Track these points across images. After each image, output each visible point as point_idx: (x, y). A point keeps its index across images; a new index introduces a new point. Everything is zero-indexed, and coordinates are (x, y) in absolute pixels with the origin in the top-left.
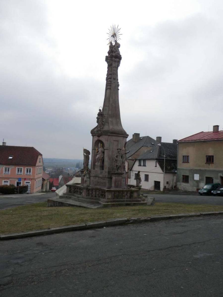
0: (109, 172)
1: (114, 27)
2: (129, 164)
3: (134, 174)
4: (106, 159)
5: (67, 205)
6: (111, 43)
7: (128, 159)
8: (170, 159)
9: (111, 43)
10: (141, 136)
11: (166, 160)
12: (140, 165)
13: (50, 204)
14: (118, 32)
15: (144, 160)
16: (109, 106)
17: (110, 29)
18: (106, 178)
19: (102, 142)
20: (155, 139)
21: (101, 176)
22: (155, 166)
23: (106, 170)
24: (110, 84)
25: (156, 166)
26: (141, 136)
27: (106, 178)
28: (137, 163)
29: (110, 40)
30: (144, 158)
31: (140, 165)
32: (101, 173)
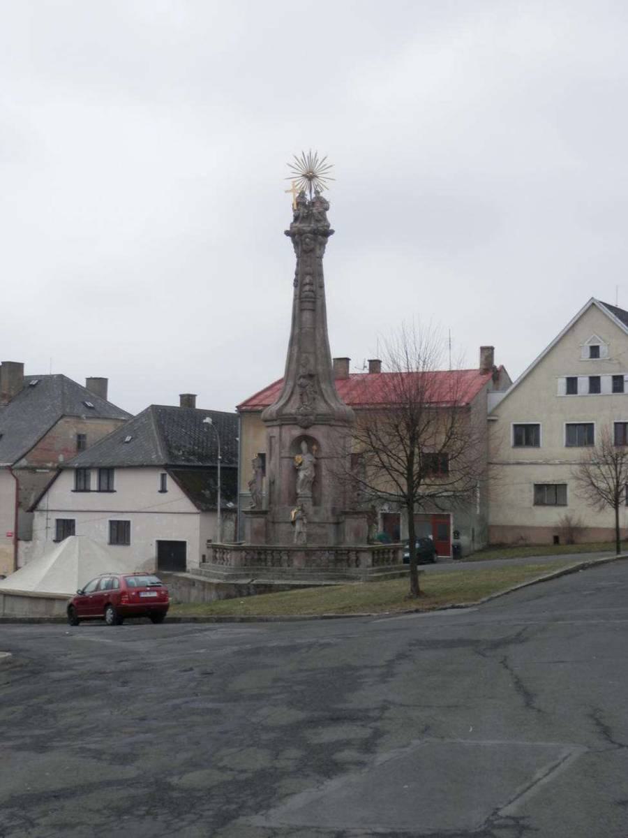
0: (334, 510)
1: (313, 155)
2: (22, 487)
3: (53, 524)
4: (326, 481)
5: (287, 589)
6: (302, 195)
7: (18, 465)
8: (200, 464)
9: (302, 195)
10: (27, 372)
11: (222, 468)
12: (82, 487)
13: (222, 593)
14: (325, 171)
15: (107, 473)
16: (315, 353)
17: (300, 157)
18: (330, 523)
19: (311, 441)
20: (83, 384)
21: (316, 520)
22: (159, 489)
23: (327, 505)
24: (313, 300)
25: (163, 490)
26: (27, 372)
27: (330, 523)
28: (67, 482)
29: (295, 181)
30: (106, 462)
31: (82, 487)
32: (316, 513)
